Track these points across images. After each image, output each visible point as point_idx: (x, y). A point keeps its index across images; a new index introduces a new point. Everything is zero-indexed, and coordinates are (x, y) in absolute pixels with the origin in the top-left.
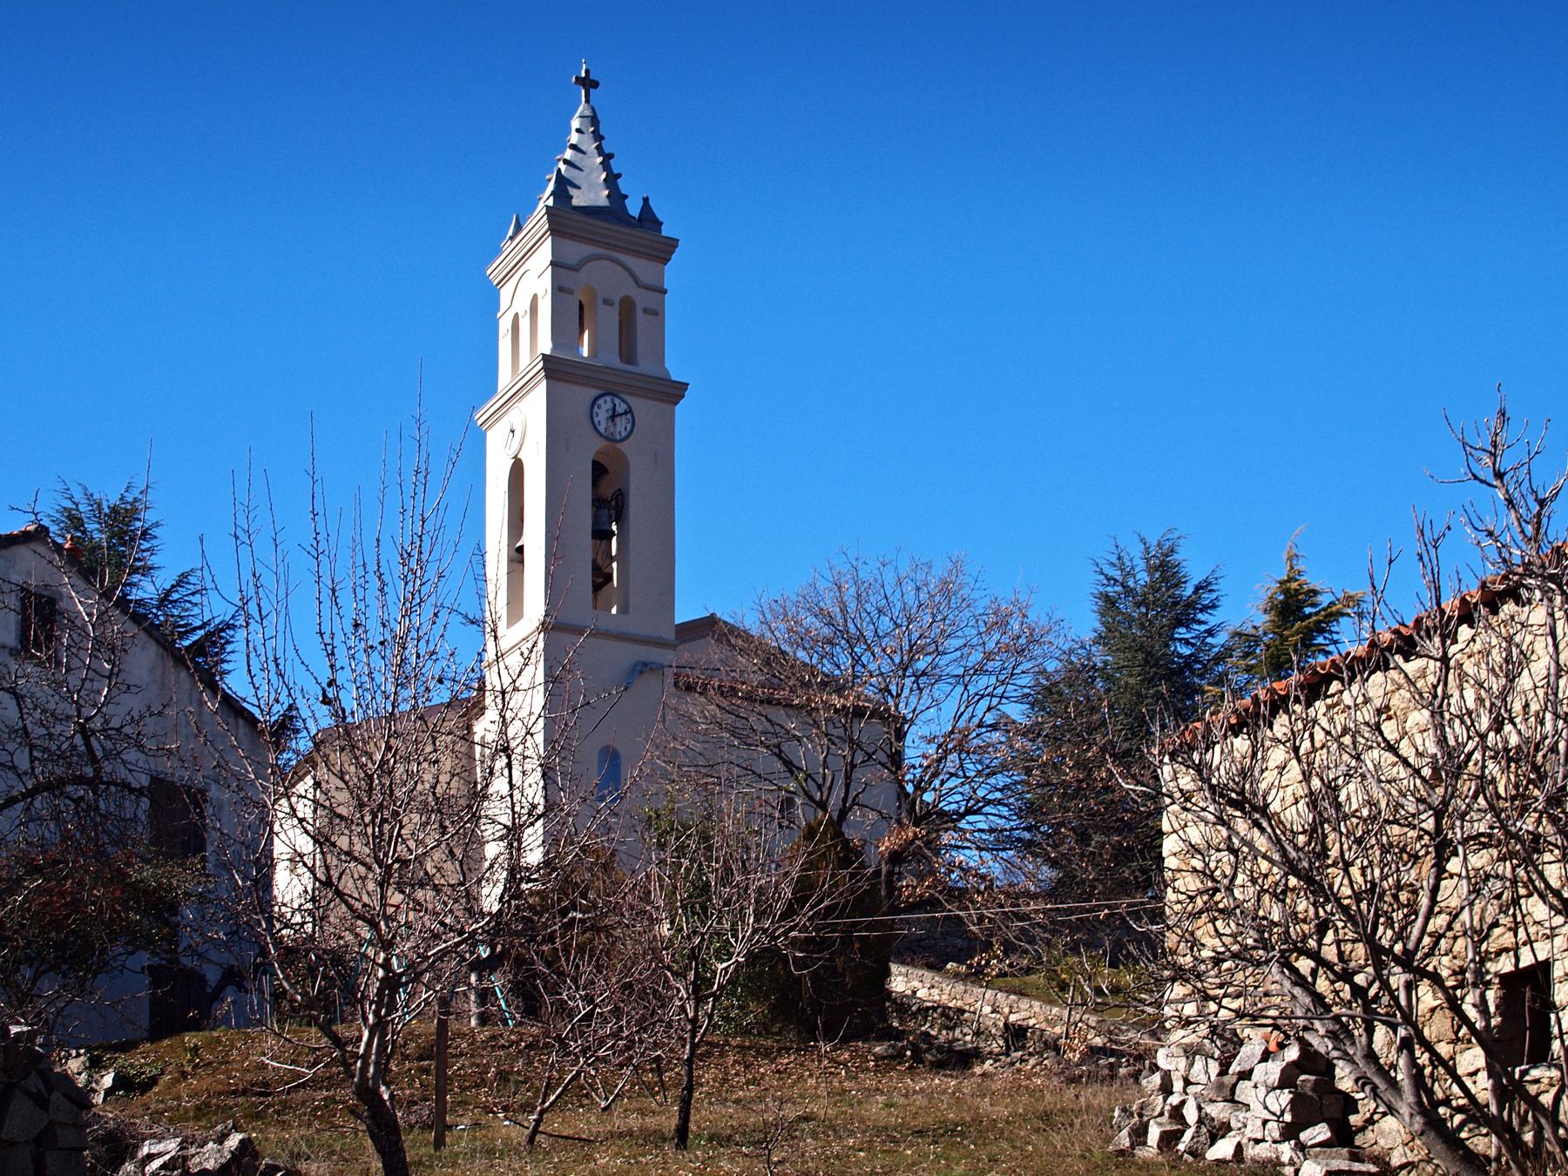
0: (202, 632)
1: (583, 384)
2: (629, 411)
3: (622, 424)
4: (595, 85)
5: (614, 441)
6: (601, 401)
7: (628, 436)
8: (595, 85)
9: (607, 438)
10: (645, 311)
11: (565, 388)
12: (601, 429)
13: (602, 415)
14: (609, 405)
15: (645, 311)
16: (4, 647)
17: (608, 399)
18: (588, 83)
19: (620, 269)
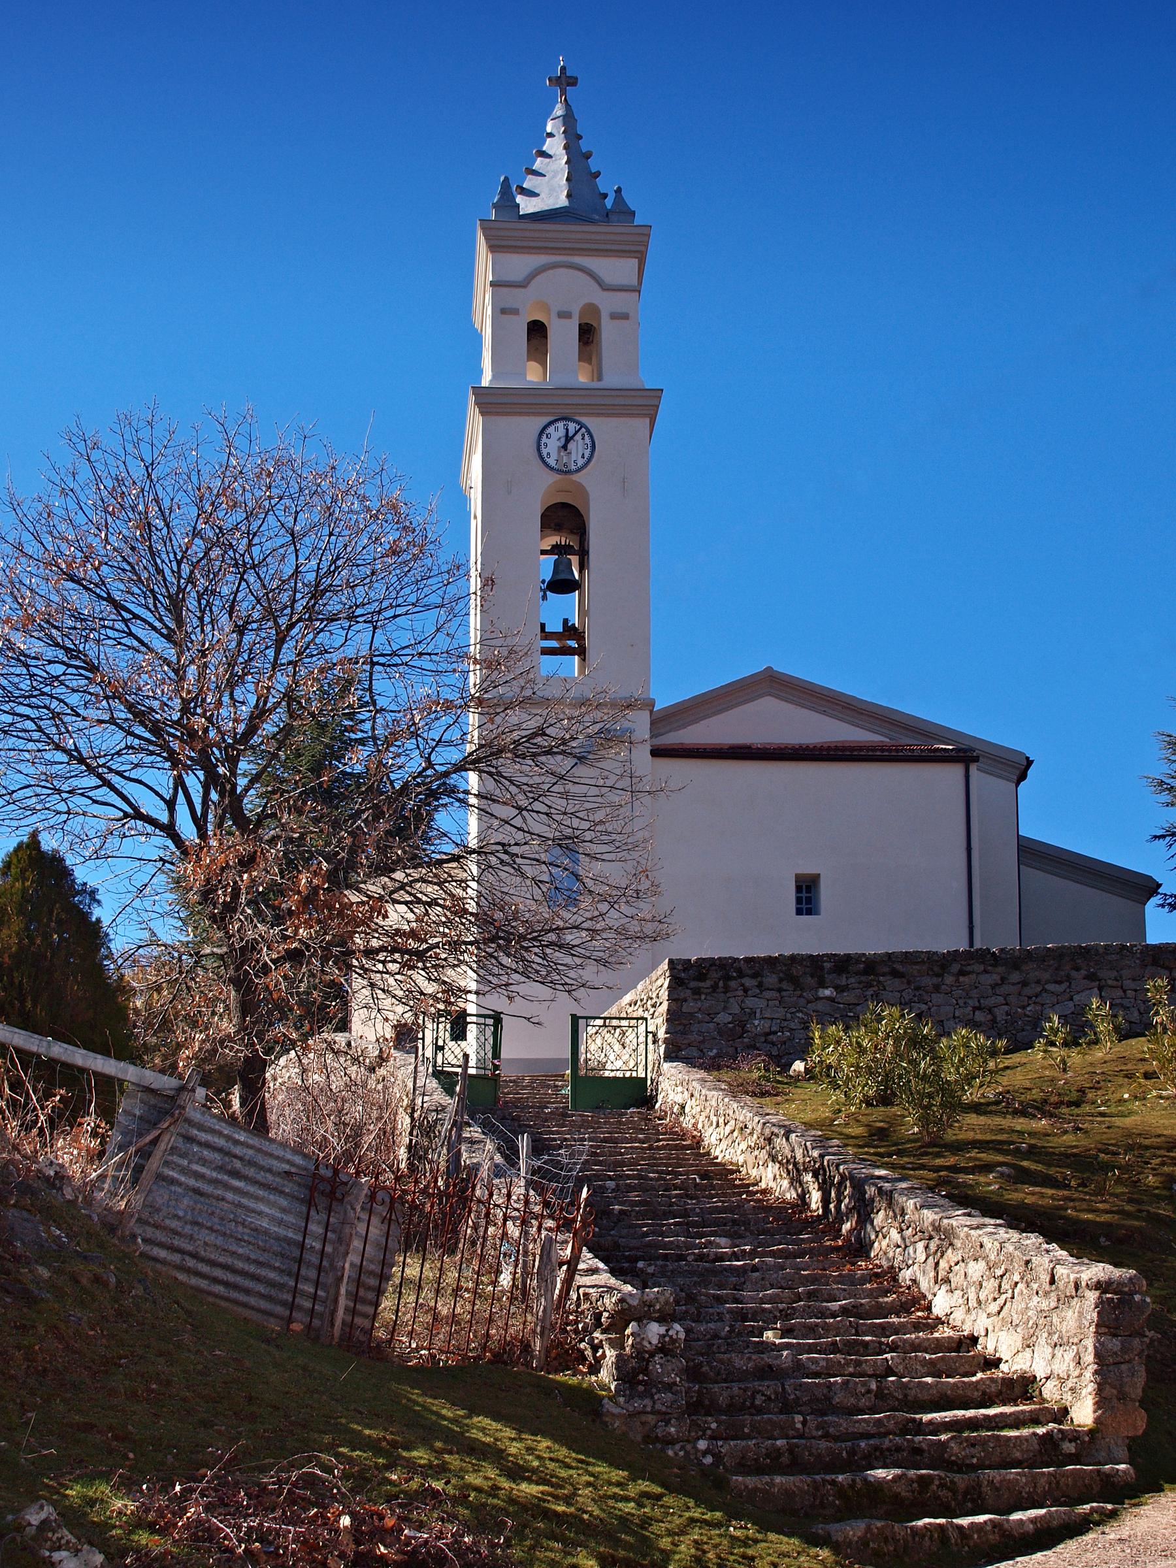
0: (924, 1160)
1: (528, 414)
2: (582, 426)
3: (578, 448)
4: (573, 82)
5: (569, 472)
6: (551, 430)
7: (539, 450)
8: (573, 82)
9: (559, 471)
10: (614, 316)
11: (503, 422)
12: (552, 462)
13: (552, 445)
14: (562, 432)
15: (614, 316)
16: (1166, 1554)
17: (560, 425)
18: (566, 81)
19: (562, 270)
